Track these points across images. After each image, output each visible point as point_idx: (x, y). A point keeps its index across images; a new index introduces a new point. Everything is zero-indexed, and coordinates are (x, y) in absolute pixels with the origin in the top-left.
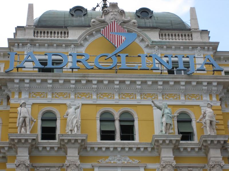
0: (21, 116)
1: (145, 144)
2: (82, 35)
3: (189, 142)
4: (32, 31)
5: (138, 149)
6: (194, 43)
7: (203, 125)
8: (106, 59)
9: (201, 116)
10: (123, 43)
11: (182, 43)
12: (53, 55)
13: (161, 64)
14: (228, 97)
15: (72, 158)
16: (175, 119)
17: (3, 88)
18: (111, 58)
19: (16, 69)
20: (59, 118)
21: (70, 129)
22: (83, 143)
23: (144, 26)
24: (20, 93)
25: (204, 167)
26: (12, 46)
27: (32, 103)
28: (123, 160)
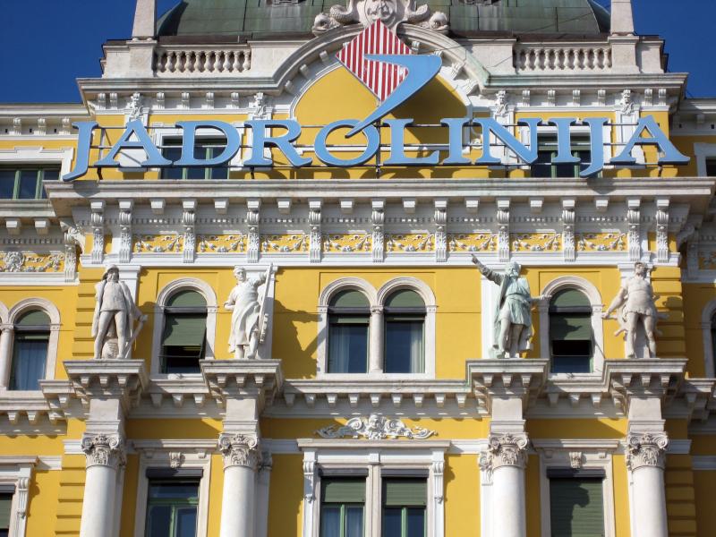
0: (103, 308)
1: (450, 383)
2: (290, 61)
3: (579, 376)
4: (149, 52)
5: (430, 398)
6: (612, 77)
7: (620, 326)
8: (347, 137)
9: (617, 299)
10: (400, 87)
11: (577, 78)
12: (198, 127)
13: (505, 146)
14: (713, 237)
15: (237, 427)
16: (543, 308)
17: (62, 224)
19: (96, 170)
20: (213, 309)
21: (238, 342)
22: (272, 385)
23: (473, 29)
24: (107, 238)
26: (91, 100)
27: (138, 268)
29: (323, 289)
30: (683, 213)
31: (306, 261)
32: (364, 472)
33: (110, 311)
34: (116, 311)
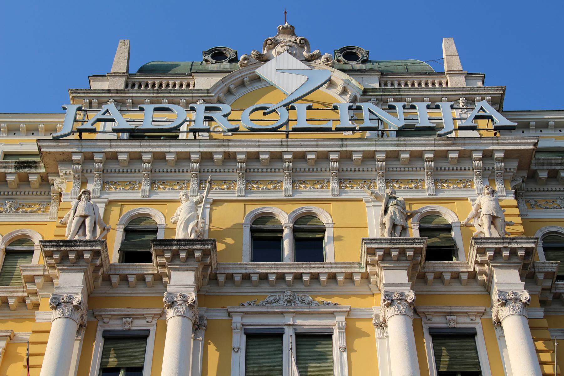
18: (277, 112)
25: (483, 313)
28: (297, 302)
29: (247, 214)
30: (514, 165)
31: (234, 196)
32: (281, 331)
33: (81, 216)
34: (85, 217)
